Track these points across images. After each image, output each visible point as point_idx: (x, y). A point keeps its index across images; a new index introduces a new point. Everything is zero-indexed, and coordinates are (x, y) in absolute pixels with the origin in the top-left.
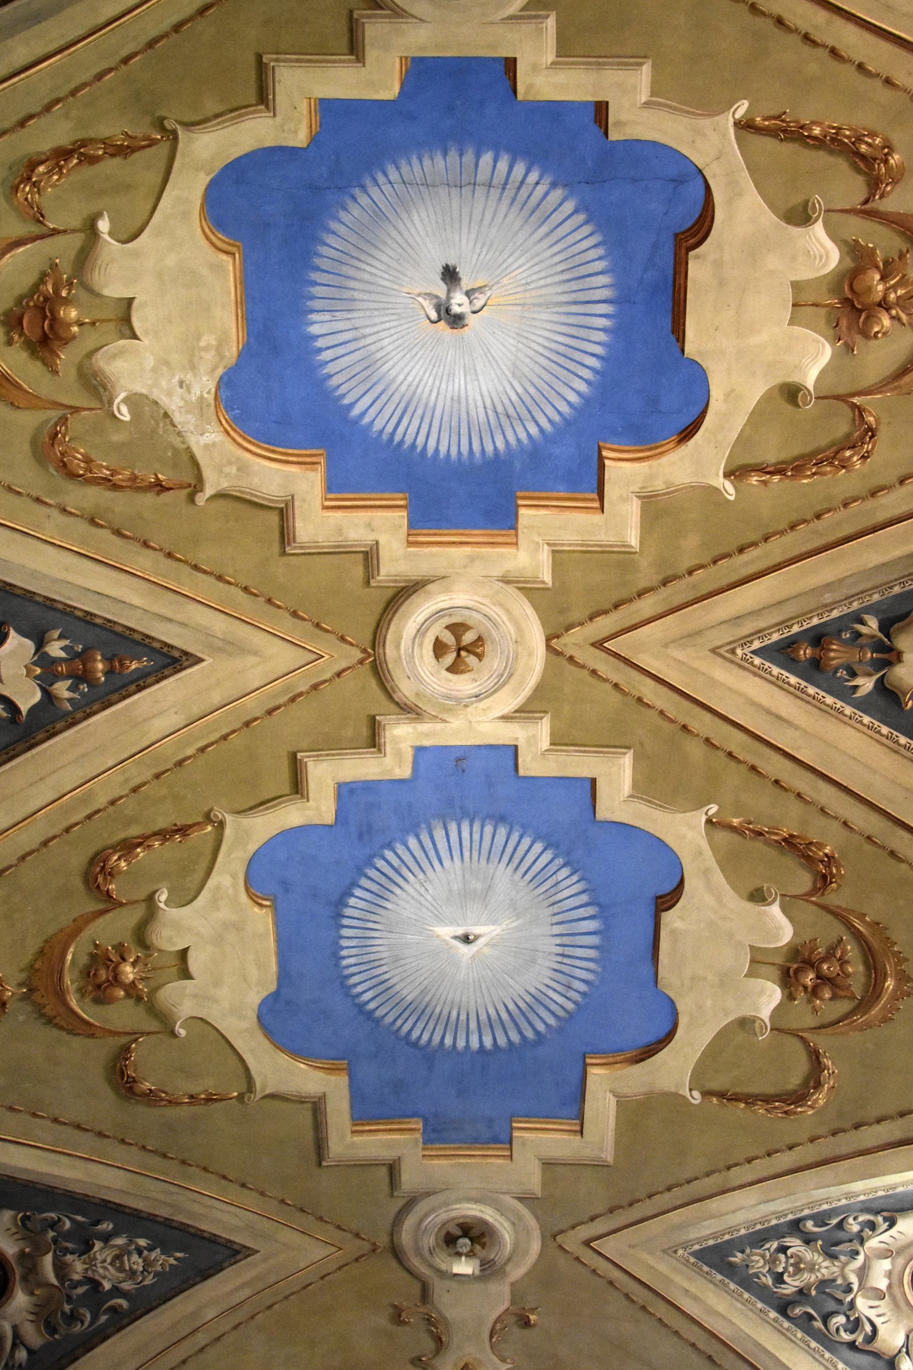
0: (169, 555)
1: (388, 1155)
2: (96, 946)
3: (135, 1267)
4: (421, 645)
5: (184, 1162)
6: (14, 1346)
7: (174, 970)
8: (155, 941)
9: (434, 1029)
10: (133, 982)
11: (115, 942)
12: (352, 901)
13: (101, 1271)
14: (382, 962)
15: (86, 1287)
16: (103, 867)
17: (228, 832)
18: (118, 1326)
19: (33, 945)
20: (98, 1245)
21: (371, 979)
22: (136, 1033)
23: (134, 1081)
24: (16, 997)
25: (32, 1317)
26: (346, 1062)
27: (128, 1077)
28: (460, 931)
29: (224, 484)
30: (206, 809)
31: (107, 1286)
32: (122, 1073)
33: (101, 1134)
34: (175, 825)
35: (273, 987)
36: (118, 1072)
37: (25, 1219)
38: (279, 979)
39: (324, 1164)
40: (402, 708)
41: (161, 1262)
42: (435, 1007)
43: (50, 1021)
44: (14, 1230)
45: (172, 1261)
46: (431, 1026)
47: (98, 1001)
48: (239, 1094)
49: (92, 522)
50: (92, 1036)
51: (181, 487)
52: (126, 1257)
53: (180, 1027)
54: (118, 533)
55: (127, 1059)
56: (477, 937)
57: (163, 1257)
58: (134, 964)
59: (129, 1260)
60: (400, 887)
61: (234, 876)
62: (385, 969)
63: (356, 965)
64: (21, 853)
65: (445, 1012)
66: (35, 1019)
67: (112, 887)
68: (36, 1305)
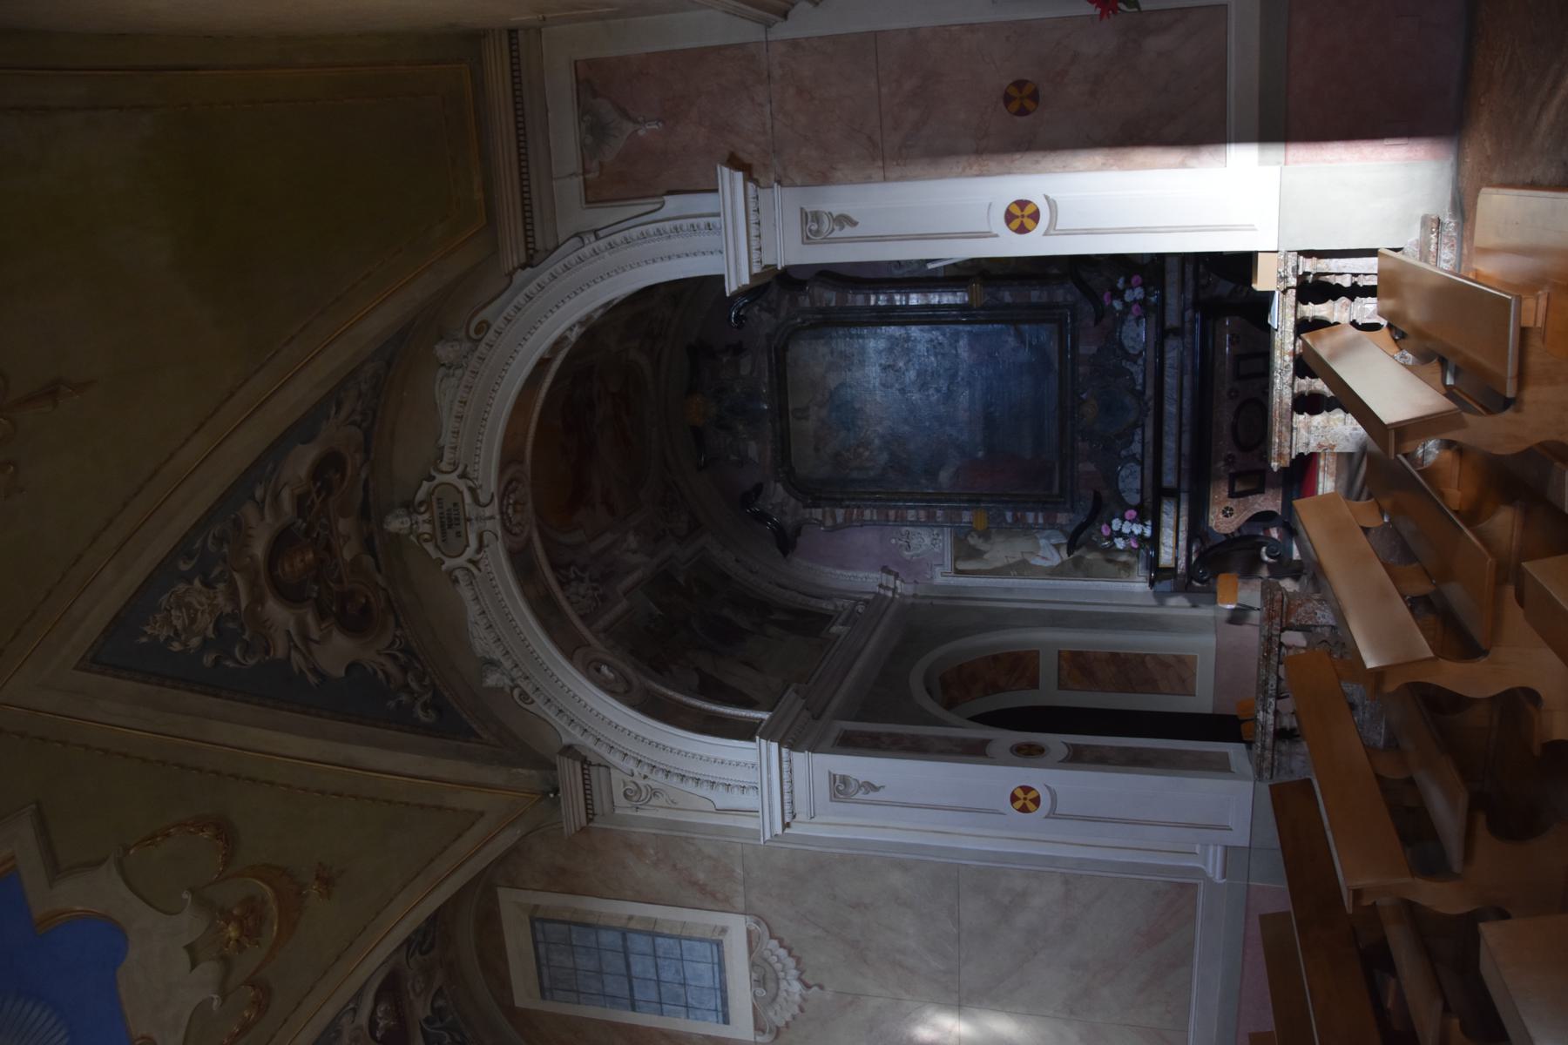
2: (258, 943)
3: (178, 614)
6: (263, 501)
10: (228, 925)
13: (204, 600)
15: (212, 576)
20: (210, 633)
27: (221, 839)
31: (197, 583)
37: (267, 652)
39: (34, 806)
41: (158, 625)
45: (147, 629)
51: (756, 191)
55: (225, 854)
57: (157, 633)
58: (230, 939)
59: (184, 620)
67: (252, 994)
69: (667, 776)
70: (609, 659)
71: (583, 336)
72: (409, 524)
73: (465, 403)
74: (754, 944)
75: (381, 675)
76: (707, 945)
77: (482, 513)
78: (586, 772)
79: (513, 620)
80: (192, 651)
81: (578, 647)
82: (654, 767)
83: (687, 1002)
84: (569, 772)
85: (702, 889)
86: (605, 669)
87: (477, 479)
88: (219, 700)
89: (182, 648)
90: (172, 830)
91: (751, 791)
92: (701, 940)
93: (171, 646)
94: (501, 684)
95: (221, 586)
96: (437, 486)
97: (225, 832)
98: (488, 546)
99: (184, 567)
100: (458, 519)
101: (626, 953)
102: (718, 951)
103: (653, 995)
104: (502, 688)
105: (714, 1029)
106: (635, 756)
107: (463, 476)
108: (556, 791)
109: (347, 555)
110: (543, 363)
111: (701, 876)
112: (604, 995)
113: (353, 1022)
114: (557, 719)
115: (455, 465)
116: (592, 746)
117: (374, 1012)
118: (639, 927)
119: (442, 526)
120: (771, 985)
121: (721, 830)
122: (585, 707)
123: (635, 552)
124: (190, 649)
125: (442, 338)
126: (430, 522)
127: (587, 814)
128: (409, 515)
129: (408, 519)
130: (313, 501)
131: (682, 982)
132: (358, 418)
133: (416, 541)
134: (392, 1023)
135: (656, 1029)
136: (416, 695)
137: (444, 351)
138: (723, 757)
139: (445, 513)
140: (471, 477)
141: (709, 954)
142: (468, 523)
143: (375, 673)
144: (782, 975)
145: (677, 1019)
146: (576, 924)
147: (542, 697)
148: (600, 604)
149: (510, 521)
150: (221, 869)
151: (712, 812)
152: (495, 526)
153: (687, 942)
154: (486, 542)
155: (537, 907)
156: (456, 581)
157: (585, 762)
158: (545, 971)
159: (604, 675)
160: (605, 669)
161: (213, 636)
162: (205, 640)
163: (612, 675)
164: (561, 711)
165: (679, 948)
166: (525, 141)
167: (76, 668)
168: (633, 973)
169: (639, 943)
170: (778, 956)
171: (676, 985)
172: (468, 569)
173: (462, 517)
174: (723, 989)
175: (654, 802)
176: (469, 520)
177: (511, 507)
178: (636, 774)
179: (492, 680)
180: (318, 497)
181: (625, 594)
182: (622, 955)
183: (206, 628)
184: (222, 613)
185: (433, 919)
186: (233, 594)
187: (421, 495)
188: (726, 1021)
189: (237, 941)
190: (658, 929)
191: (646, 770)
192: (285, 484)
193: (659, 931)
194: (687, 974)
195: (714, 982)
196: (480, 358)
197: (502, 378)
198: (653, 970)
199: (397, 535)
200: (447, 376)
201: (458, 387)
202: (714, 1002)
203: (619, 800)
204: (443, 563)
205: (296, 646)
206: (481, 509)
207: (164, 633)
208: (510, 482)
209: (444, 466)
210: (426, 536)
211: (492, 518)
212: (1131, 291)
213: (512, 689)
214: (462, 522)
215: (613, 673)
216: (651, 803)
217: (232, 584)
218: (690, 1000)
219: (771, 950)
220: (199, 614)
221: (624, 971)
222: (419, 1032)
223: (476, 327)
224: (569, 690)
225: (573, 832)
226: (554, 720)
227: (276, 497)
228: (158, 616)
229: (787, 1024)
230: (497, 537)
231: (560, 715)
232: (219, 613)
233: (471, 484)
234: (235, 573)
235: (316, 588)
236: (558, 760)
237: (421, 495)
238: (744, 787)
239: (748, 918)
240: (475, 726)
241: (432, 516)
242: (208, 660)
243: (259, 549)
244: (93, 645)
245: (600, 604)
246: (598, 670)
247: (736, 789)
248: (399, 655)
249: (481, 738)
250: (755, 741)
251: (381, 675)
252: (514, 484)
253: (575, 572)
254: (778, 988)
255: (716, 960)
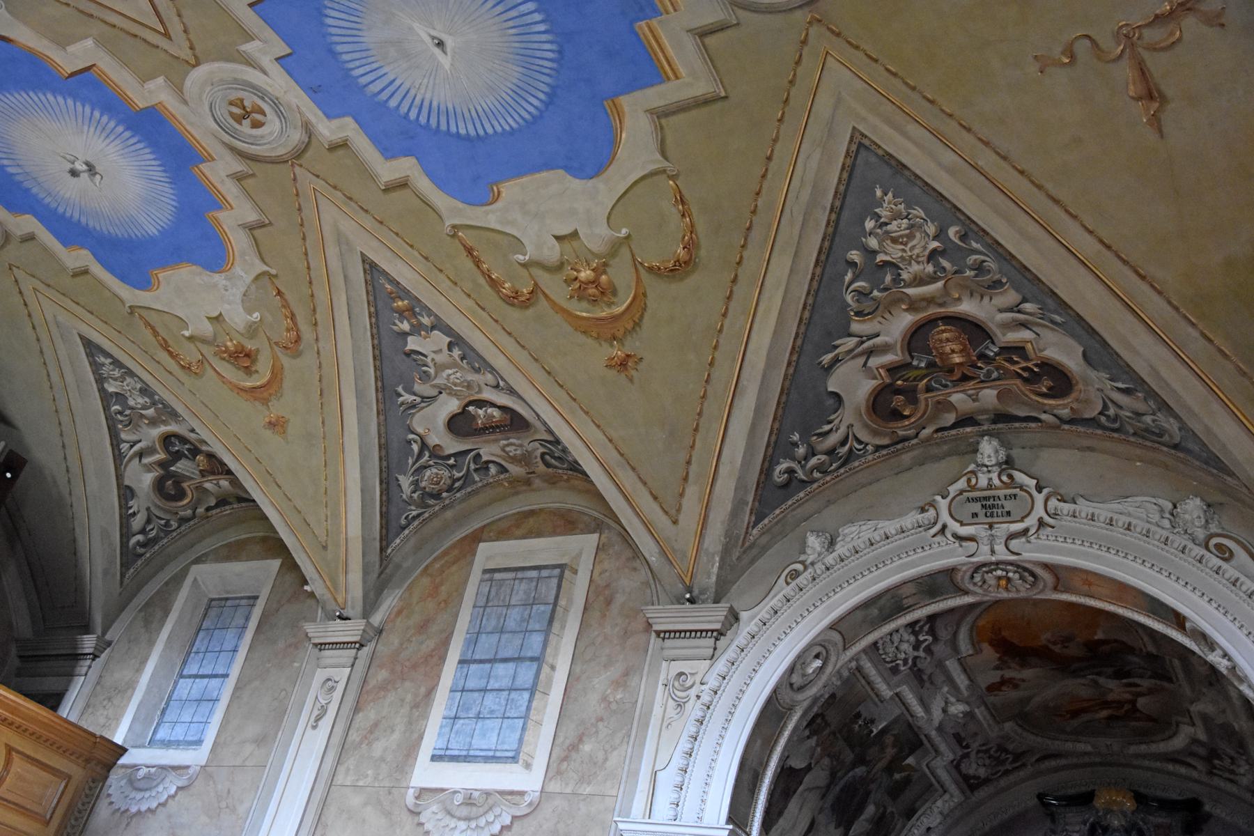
0: (310, 283)
1: (690, 43)
2: (571, 297)
4: (262, 137)
5: (754, 212)
6: (1019, 312)
7: (575, 244)
8: (555, 260)
9: (536, 42)
10: (593, 270)
11: (564, 285)
12: (462, 131)
13: (916, 251)
14: (499, 98)
15: (941, 260)
16: (513, 298)
17: (457, 222)
18: (981, 233)
19: (582, 338)
21: (519, 104)
22: (635, 264)
23: (678, 261)
24: (621, 347)
25: (986, 299)
26: (605, 103)
28: (437, 51)
29: (257, 261)
30: (449, 238)
31: (935, 244)
32: (672, 270)
33: (734, 281)
34: (467, 256)
35: (561, 172)
36: (670, 274)
37: (858, 314)
38: (552, 169)
39: (723, 94)
40: (310, 135)
41: (893, 207)
42: (515, 48)
43: (637, 324)
44: (880, 319)
46: (535, 46)
47: (614, 293)
48: (670, 179)
49: (316, 324)
50: (645, 295)
51: (273, 283)
52: (893, 235)
53: (620, 233)
54: (314, 310)
55: (659, 269)
56: (433, 38)
57: (885, 205)
58: (578, 271)
60: (431, 103)
61: (487, 213)
62: (504, 95)
63: (512, 117)
64: (520, 348)
65: (517, 38)
66: (637, 334)
67: (525, 291)
68: (972, 295)
69: (698, 721)
70: (829, 669)
71: (1213, 669)
72: (988, 463)
73: (1128, 529)
74: (510, 797)
75: (827, 428)
76: (515, 746)
77: (998, 541)
78: (709, 634)
79: (878, 568)
80: (864, 240)
81: (844, 639)
82: (708, 708)
83: (459, 718)
84: (712, 616)
85: (574, 747)
86: (818, 663)
87: (1038, 538)
88: (812, 265)
89: (867, 230)
90: (688, 219)
91: (672, 813)
92: (521, 741)
93: (871, 219)
94: (809, 551)
95: (930, 268)
96: (1031, 496)
97: (680, 269)
98: (961, 546)
99: (952, 232)
100: (992, 516)
101: (518, 659)
102: (507, 757)
103: (471, 684)
104: (804, 553)
105: (430, 743)
106: (722, 688)
107: (1041, 523)
108: (692, 601)
109: (957, 398)
110: (1179, 621)
111: (587, 747)
112: (478, 633)
113: (486, 385)
114: (768, 607)
115: (1054, 516)
116: (736, 643)
117: (493, 405)
118: (542, 676)
119: (985, 498)
120: (464, 811)
121: (634, 774)
122: (779, 639)
123: (944, 711)
124: (866, 238)
125: (1209, 506)
126: (990, 487)
127: (665, 632)
128: (999, 464)
129: (993, 462)
130: (1017, 363)
131: (482, 716)
132: (1112, 411)
133: (969, 469)
134: (480, 422)
135: (437, 684)
136: (803, 462)
137: (1193, 508)
138: (713, 785)
139: (1000, 503)
140: (1040, 532)
141: (506, 747)
142: (987, 526)
143: (830, 422)
144: (473, 824)
145: (444, 706)
146: (553, 611)
147: (792, 594)
148: (890, 665)
149: (987, 572)
150: (646, 265)
151: (654, 766)
152: (984, 556)
153: (521, 725)
154: (964, 544)
155: (575, 572)
156: (923, 510)
157: (721, 633)
158: (511, 575)
159: (811, 662)
160: (818, 663)
161: (878, 260)
162: (874, 253)
163: (811, 671)
164: (776, 612)
165: (515, 716)
166: (680, 637)
167: (854, 128)
168: (497, 665)
169: (526, 674)
170: (492, 823)
171: (478, 709)
172: (935, 523)
173: (995, 520)
174: (467, 759)
175: (671, 703)
176: (991, 526)
177: (1004, 573)
178: (703, 687)
179: (814, 542)
180: (1021, 368)
181: (897, 694)
182: (516, 656)
183: (886, 254)
184: (902, 269)
185: (575, 468)
186: (919, 281)
187: (1020, 477)
188: (434, 758)
189: (576, 279)
190: (538, 695)
191: (706, 698)
192: (1038, 335)
193: (536, 696)
194: (488, 721)
195: (477, 750)
196: (1184, 548)
197: (1160, 572)
198: (497, 686)
199: (976, 451)
200: (1162, 511)
201: (1148, 522)
202: (456, 748)
203: (677, 667)
204: (943, 498)
205: (863, 342)
206: (1003, 541)
207: (884, 213)
208: (1033, 574)
209: (1053, 503)
210: (974, 481)
211: (993, 552)
212: (967, 759)
213: (802, 563)
214: (990, 520)
215: (813, 672)
216: (670, 700)
217: (933, 279)
218: (461, 721)
219: (500, 815)
220: (903, 247)
221: (499, 657)
222: (469, 448)
223: (1223, 545)
224: (797, 623)
225: (648, 615)
226: (767, 605)
227: (1024, 325)
228: (902, 206)
229: (422, 824)
230: (969, 556)
231: (772, 612)
232: (901, 265)
233: (1032, 531)
234: (943, 282)
235: (923, 365)
236: (724, 606)
237: (1020, 477)
238: (678, 805)
239: (538, 794)
240: (766, 521)
241: (996, 488)
242: (855, 255)
243: (967, 307)
244: (875, 144)
245: (890, 665)
246: (817, 656)
247: (676, 796)
248: (847, 447)
249: (753, 527)
250: (727, 823)
251: (827, 428)
252: (1031, 579)
253: (926, 640)
254: (460, 819)
255: (498, 754)
